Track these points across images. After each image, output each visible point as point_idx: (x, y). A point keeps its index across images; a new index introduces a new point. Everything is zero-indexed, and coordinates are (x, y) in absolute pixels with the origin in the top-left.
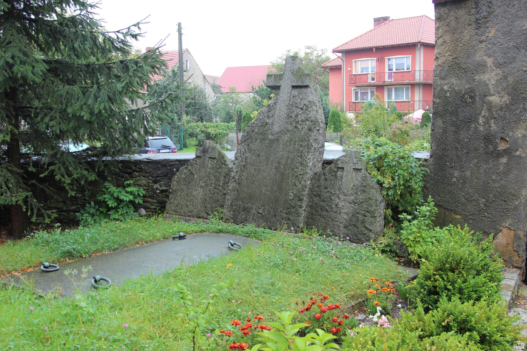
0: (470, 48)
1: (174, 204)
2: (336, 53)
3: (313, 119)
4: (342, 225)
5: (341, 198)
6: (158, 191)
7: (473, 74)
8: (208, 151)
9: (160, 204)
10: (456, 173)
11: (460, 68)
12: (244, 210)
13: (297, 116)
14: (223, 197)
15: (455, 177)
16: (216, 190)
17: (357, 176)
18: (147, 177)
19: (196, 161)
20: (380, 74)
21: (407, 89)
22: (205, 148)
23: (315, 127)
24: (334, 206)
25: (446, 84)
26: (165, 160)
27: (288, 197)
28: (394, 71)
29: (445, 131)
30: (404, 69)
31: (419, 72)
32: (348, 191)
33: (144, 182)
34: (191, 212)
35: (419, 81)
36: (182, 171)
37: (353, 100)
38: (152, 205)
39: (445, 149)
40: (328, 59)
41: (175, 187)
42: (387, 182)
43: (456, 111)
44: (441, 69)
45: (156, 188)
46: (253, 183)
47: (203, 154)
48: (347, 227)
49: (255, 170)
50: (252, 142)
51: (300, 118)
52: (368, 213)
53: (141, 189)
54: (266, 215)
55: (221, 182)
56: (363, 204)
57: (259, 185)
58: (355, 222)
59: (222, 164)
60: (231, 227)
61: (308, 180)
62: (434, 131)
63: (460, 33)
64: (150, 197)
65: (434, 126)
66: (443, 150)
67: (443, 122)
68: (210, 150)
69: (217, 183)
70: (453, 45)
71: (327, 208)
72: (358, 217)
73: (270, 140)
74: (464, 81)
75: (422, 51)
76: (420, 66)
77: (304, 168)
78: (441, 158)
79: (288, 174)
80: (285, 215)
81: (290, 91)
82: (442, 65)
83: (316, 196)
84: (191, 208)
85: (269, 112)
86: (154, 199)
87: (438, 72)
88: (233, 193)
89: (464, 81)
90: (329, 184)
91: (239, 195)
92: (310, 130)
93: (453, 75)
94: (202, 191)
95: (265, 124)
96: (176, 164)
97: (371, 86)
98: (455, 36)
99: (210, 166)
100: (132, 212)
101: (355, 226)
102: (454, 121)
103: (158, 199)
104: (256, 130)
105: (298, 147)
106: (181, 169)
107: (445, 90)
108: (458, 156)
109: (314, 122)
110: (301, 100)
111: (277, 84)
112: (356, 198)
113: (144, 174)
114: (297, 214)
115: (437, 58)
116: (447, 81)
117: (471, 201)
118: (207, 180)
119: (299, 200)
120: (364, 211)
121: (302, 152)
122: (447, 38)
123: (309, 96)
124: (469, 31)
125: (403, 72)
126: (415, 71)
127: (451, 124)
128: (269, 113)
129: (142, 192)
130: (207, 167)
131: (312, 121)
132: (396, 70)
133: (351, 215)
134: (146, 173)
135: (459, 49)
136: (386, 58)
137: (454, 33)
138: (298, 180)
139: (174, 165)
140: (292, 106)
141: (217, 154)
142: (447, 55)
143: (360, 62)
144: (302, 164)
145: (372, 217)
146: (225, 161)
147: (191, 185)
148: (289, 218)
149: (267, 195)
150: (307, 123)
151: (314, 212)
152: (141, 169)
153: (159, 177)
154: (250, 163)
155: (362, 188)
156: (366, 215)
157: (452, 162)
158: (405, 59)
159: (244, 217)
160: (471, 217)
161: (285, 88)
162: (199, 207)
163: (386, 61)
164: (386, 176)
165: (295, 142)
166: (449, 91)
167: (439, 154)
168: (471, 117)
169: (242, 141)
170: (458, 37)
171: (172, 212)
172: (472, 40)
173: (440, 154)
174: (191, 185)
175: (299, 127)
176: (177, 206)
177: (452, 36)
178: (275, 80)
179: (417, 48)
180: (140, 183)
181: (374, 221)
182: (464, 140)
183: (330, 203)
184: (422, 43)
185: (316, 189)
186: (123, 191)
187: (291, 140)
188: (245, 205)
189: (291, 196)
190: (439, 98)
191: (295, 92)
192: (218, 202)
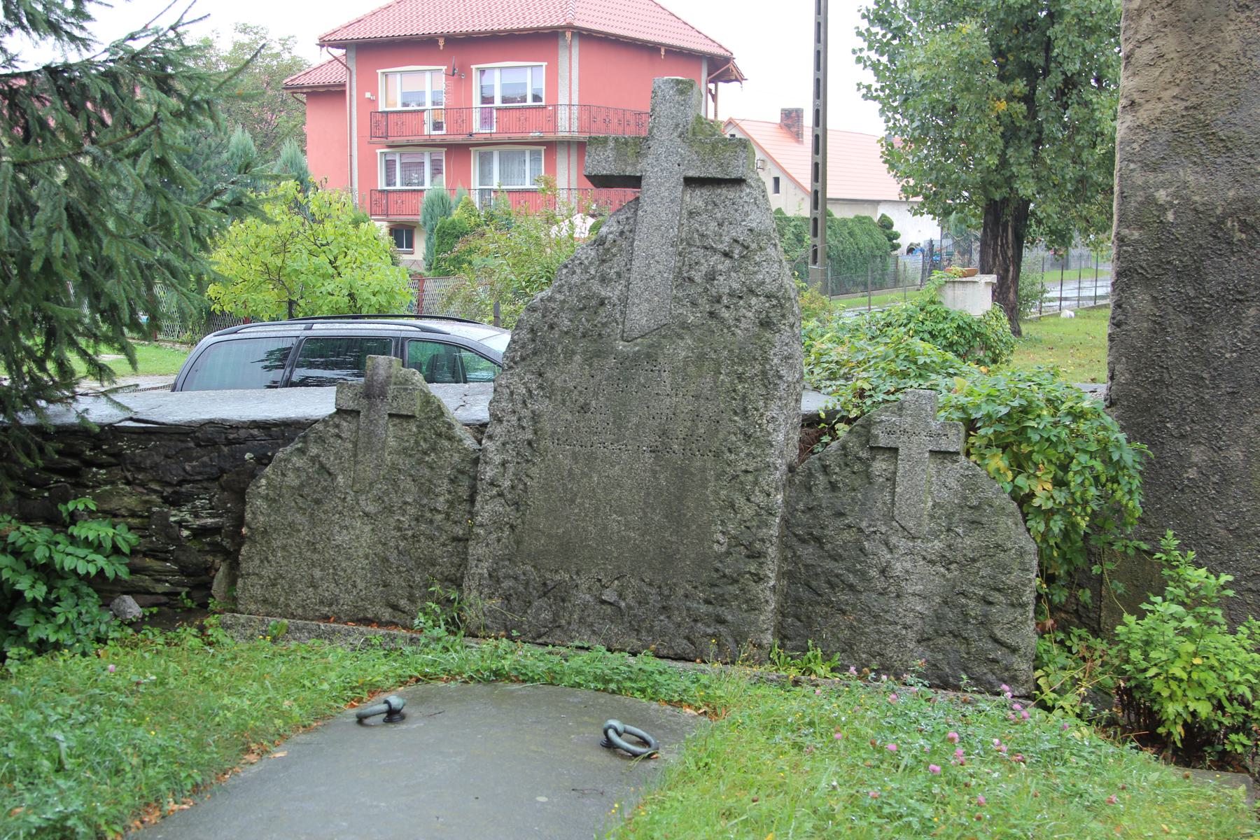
0: (1243, 79)
1: (260, 577)
2: (330, 49)
3: (770, 287)
4: (910, 634)
5: (896, 547)
6: (185, 533)
7: (1252, 156)
8: (383, 394)
9: (188, 575)
10: (1198, 455)
11: (1209, 136)
12: (545, 594)
13: (711, 277)
14: (450, 548)
15: (1192, 465)
16: (423, 527)
17: (944, 474)
18: (142, 485)
19: (337, 426)
20: (459, 112)
21: (535, 157)
22: (373, 380)
23: (783, 316)
24: (874, 573)
25: (1163, 185)
26: (211, 423)
27: (711, 548)
28: (498, 103)
29: (1159, 327)
30: (525, 101)
31: (567, 109)
32: (920, 525)
33: (131, 502)
34: (331, 605)
35: (567, 134)
36: (287, 460)
37: (382, 185)
38: (158, 581)
39: (1161, 381)
40: (294, 66)
41: (261, 518)
42: (1043, 491)
43: (1197, 268)
44: (1146, 137)
45: (180, 524)
46: (573, 501)
47: (365, 402)
48: (929, 639)
49: (575, 457)
50: (553, 363)
51: (723, 285)
52: (997, 594)
53: (122, 529)
54: (629, 607)
55: (441, 499)
56: (977, 565)
57: (597, 509)
58: (957, 623)
59: (439, 435)
60: (528, 656)
61: (777, 489)
62: (1124, 327)
63: (1211, 31)
64: (152, 553)
65: (1125, 312)
66: (1154, 383)
67: (1155, 299)
68: (391, 390)
69: (425, 501)
70: (1190, 68)
71: (852, 579)
72: (963, 606)
73: (623, 359)
74: (1221, 178)
75: (575, 51)
76: (569, 93)
77: (759, 452)
78: (1148, 409)
79: (703, 470)
80: (704, 608)
81: (679, 194)
82: (1152, 127)
83: (803, 541)
84: (328, 588)
85: (604, 261)
86: (166, 560)
87: (1135, 145)
88: (494, 536)
89: (1221, 178)
90: (847, 499)
91: (518, 543)
92: (766, 324)
93: (1186, 157)
94: (367, 529)
95: (593, 303)
96: (254, 437)
97: (431, 145)
98: (1196, 38)
99: (392, 442)
100: (95, 610)
101: (955, 636)
102: (1190, 299)
103: (183, 558)
104: (565, 323)
105: (732, 383)
106: (279, 455)
107: (1161, 202)
108: (1201, 402)
109: (777, 298)
110: (721, 225)
111: (629, 171)
112: (949, 546)
113: (128, 474)
114: (747, 602)
115: (1133, 103)
116: (1168, 176)
117: (1248, 536)
118: (386, 493)
119: (748, 557)
120: (983, 586)
121: (744, 398)
122: (1169, 43)
123: (747, 214)
124: (1242, 26)
125: (519, 108)
126: (555, 106)
127: (1179, 306)
128: (605, 267)
129: (127, 538)
130: (383, 449)
131: (768, 297)
132: (504, 100)
133: (938, 600)
134: (140, 469)
135: (1208, 81)
136: (473, 67)
137: (1191, 31)
138: (742, 490)
139: (246, 440)
140: (689, 244)
141: (418, 402)
142: (1166, 95)
143: (398, 76)
144: (750, 437)
145: (1013, 605)
146: (450, 426)
147: (325, 512)
148: (718, 616)
149: (627, 543)
150: (754, 301)
151: (803, 593)
152: (118, 455)
153: (189, 482)
154: (554, 433)
155: (967, 514)
156: (991, 599)
157: (1184, 419)
158: (529, 71)
159: (546, 615)
160: (1250, 585)
161: (661, 185)
162: (361, 585)
163: (476, 76)
164: (1038, 473)
165: (718, 364)
166: (1172, 206)
167: (1139, 395)
168: (1247, 286)
169: (513, 360)
170: (1204, 43)
171: (253, 607)
172: (1249, 54)
173: (1145, 395)
174: (325, 512)
175: (725, 314)
176: (274, 585)
177: (1185, 39)
178: (620, 156)
179: (561, 43)
180: (113, 504)
181: (1020, 619)
182: (1223, 355)
183: (860, 563)
184: (576, 28)
185: (804, 518)
186: (60, 537)
187: (702, 357)
188: (548, 575)
189: (720, 542)
190: (1141, 228)
191: (697, 198)
192: (434, 565)
